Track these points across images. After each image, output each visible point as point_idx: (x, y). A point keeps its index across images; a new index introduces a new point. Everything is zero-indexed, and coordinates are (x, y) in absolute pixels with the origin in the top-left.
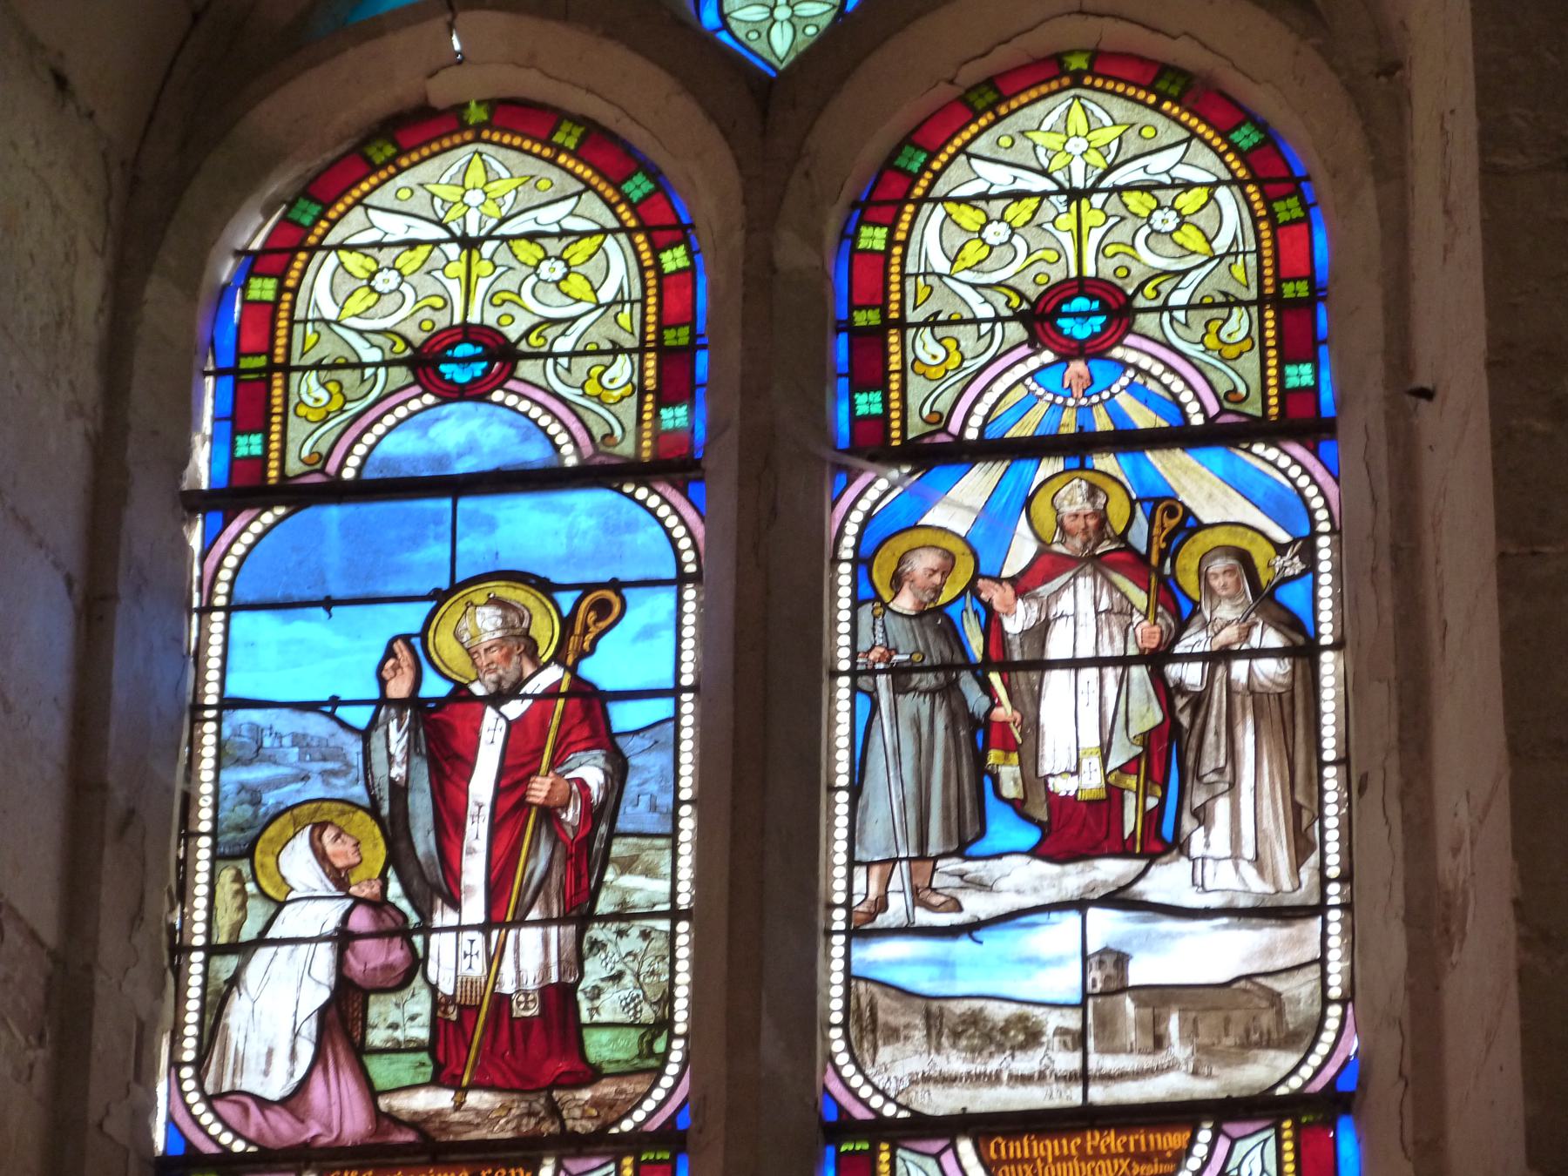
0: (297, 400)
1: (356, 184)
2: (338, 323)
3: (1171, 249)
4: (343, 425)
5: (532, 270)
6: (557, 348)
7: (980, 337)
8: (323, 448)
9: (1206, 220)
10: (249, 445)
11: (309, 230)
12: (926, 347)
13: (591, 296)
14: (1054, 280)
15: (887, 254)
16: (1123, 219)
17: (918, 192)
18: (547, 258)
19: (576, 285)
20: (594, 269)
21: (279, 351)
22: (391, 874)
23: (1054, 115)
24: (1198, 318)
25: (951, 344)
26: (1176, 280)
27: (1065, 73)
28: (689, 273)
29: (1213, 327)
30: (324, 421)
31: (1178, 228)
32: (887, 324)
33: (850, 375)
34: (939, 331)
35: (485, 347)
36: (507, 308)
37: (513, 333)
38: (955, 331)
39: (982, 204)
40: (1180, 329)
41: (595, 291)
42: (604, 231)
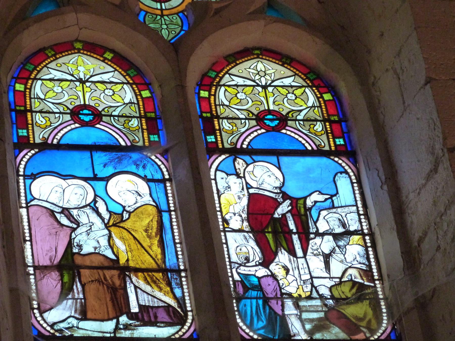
0: (35, 122)
1: (44, 61)
2: (44, 99)
3: (294, 104)
4: (51, 130)
5: (285, 96)
6: (114, 113)
7: (56, 118)
9: (122, 93)
10: (340, 141)
11: (31, 73)
13: (122, 101)
14: (261, 110)
15: (25, 92)
16: (96, 90)
18: (107, 89)
19: (116, 97)
20: (122, 93)
21: (28, 106)
23: (73, 60)
24: (122, 120)
25: (47, 119)
26: (298, 113)
27: (74, 49)
28: (152, 98)
30: (45, 128)
31: (113, 95)
34: (44, 115)
35: (92, 112)
36: (280, 106)
37: (100, 109)
38: (235, 121)
39: (235, 87)
40: (303, 126)
41: (123, 100)
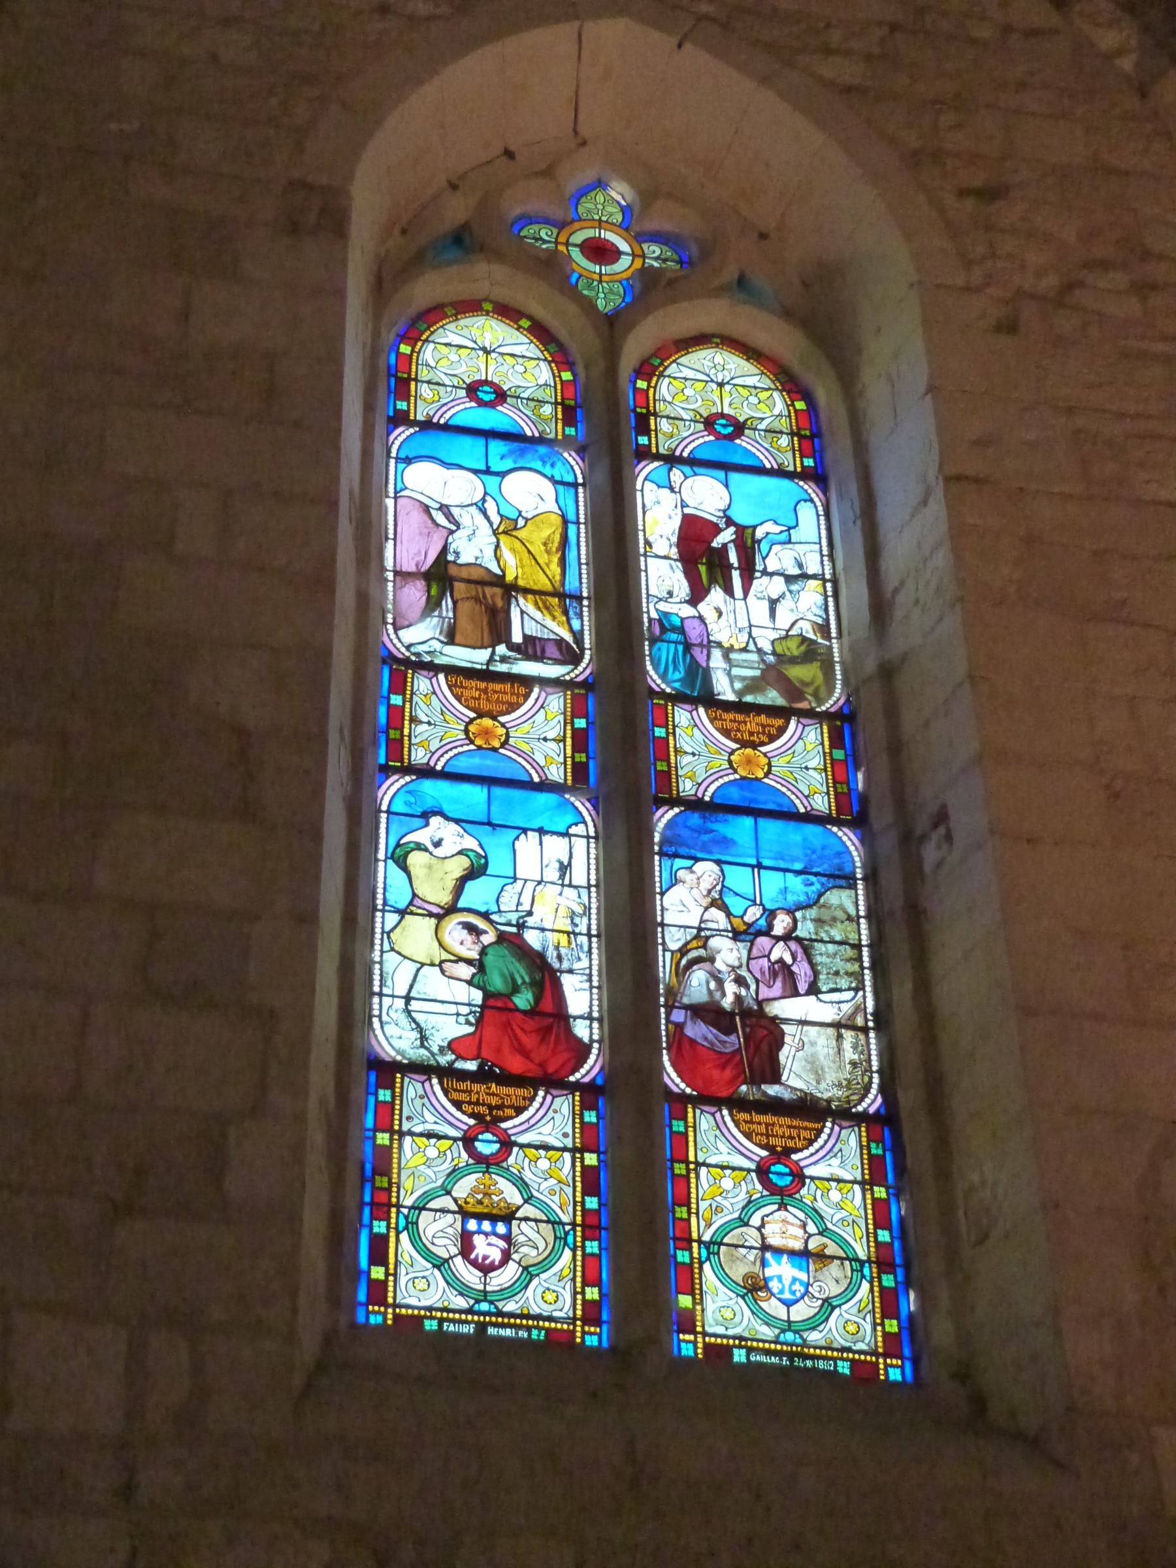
8: (431, 413)
12: (425, 391)
17: (424, 337)
20: (537, 372)
22: (500, 573)
24: (532, 404)
25: (436, 393)
29: (775, 439)
32: (649, 414)
33: (635, 428)
34: (432, 386)
42: (538, 359)
